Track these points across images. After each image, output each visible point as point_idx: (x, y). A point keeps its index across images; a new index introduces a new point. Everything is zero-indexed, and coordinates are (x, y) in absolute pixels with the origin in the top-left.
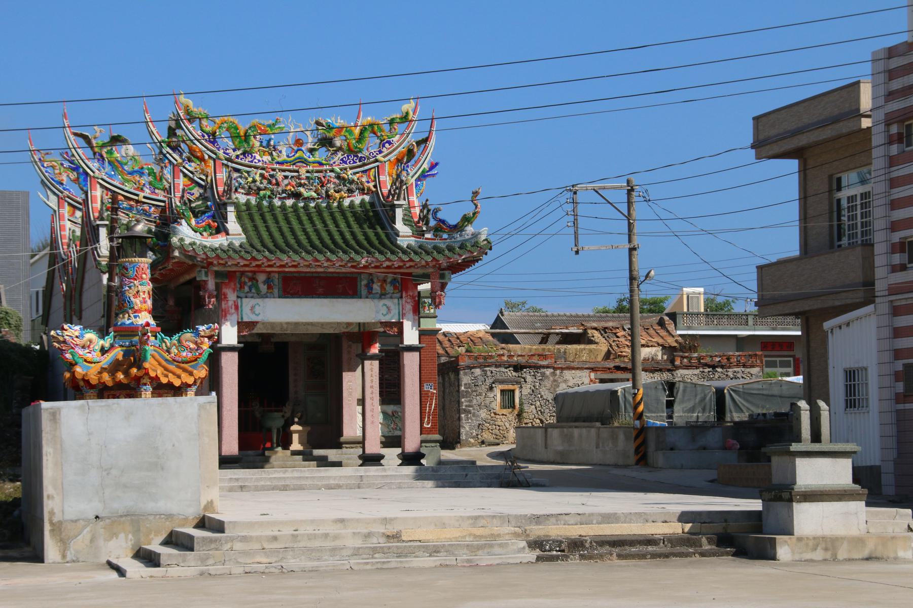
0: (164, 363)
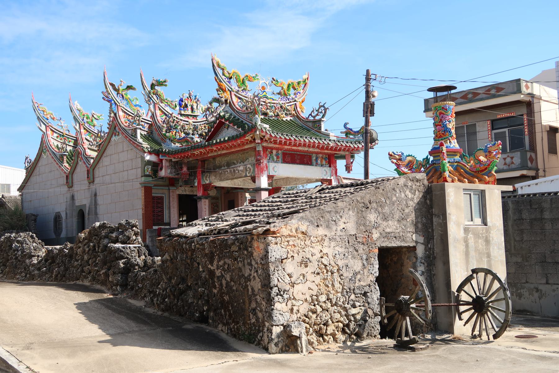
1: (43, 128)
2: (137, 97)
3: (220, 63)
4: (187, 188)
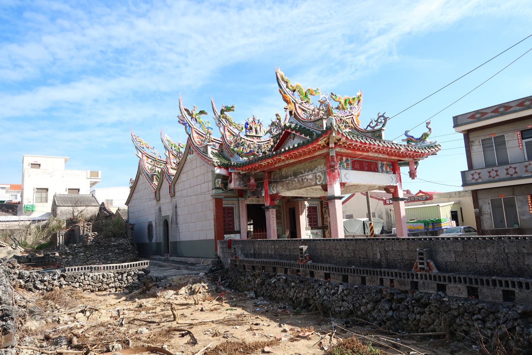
1: (140, 155)
2: (209, 120)
3: (284, 77)
4: (254, 199)
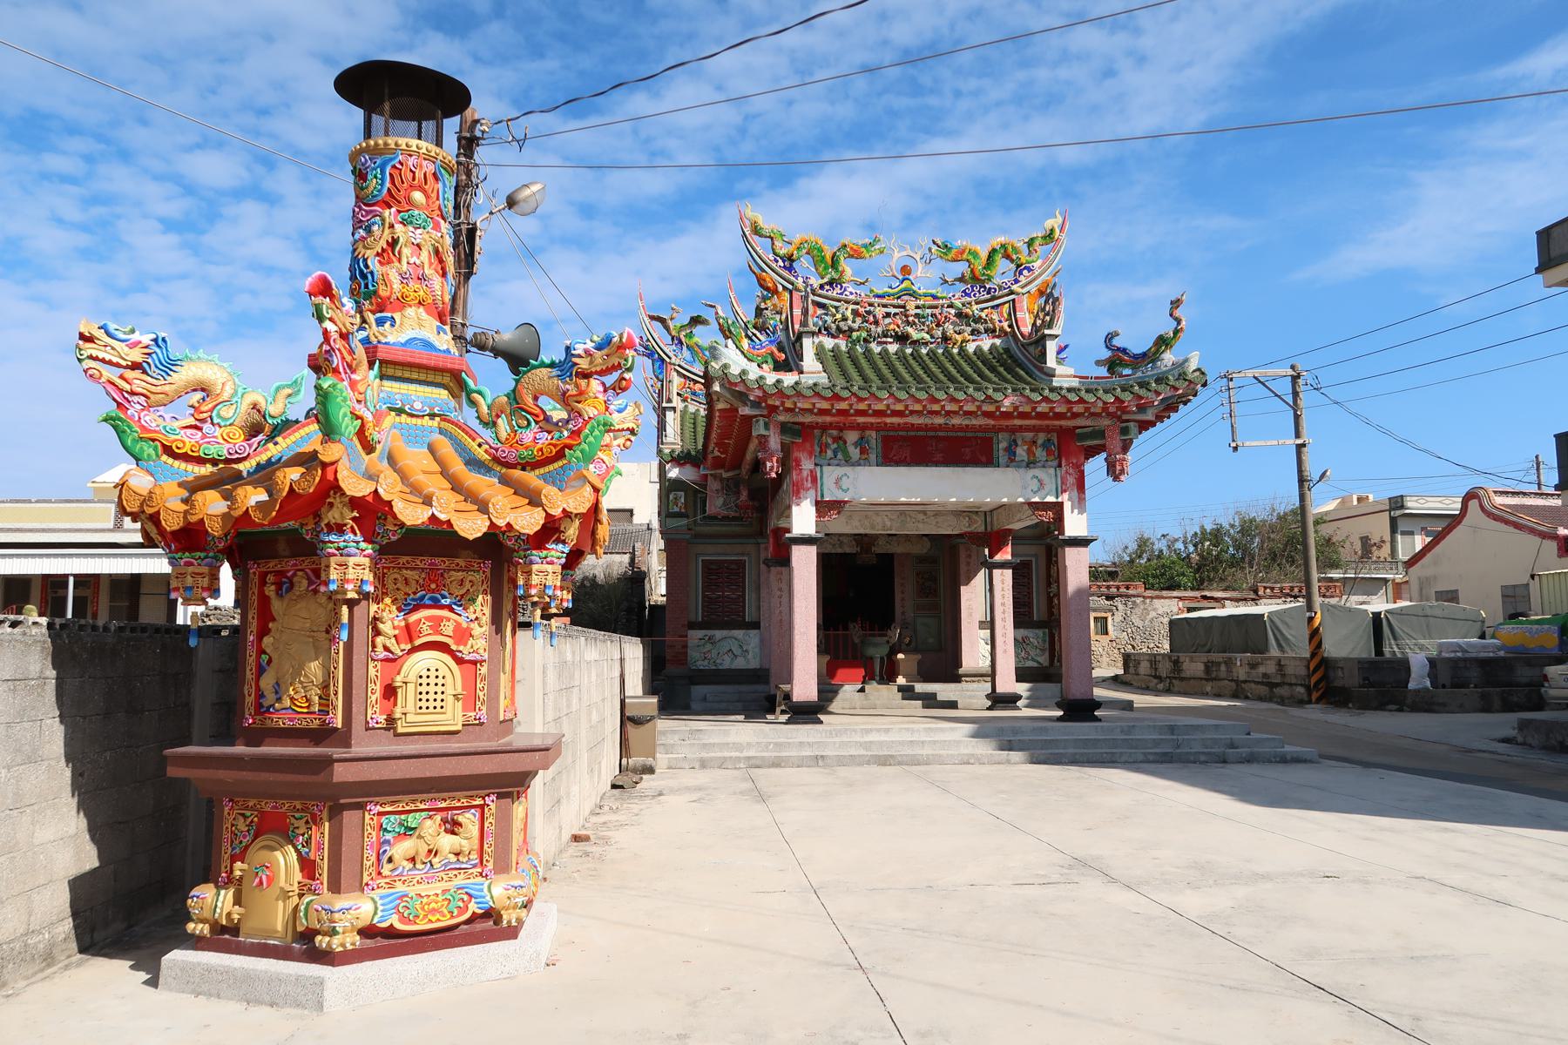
0: (458, 467)
3: (761, 223)
